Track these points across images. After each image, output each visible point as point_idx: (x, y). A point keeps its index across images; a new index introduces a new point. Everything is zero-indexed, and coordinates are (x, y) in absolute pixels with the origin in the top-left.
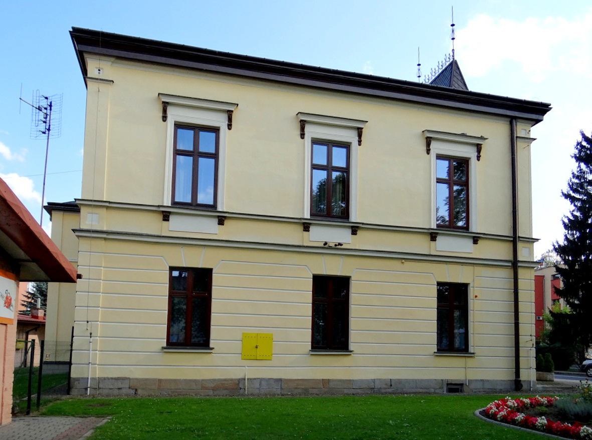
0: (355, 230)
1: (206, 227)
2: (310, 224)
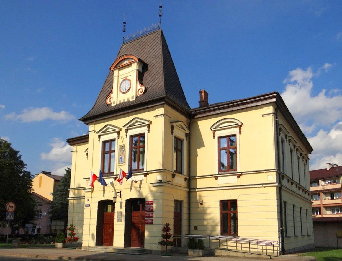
0: (239, 176)
1: (232, 180)
2: (218, 177)
